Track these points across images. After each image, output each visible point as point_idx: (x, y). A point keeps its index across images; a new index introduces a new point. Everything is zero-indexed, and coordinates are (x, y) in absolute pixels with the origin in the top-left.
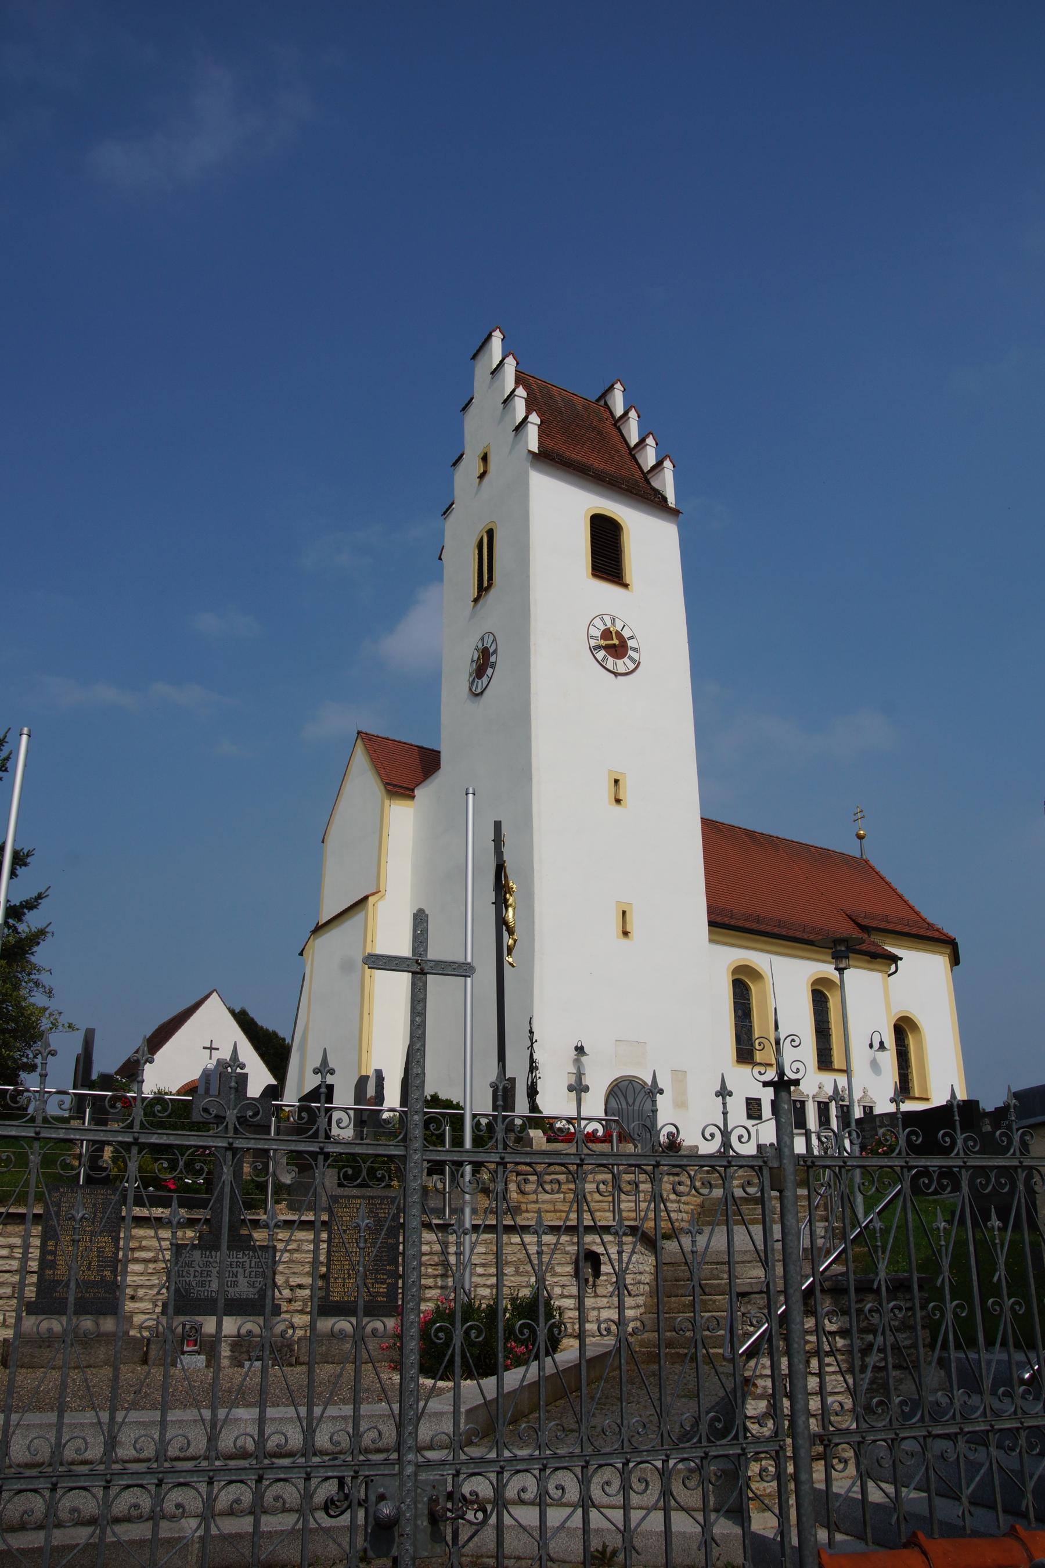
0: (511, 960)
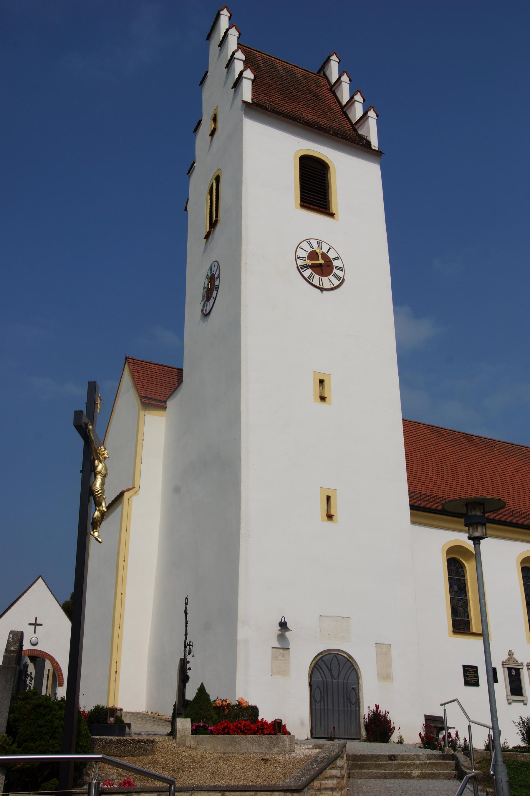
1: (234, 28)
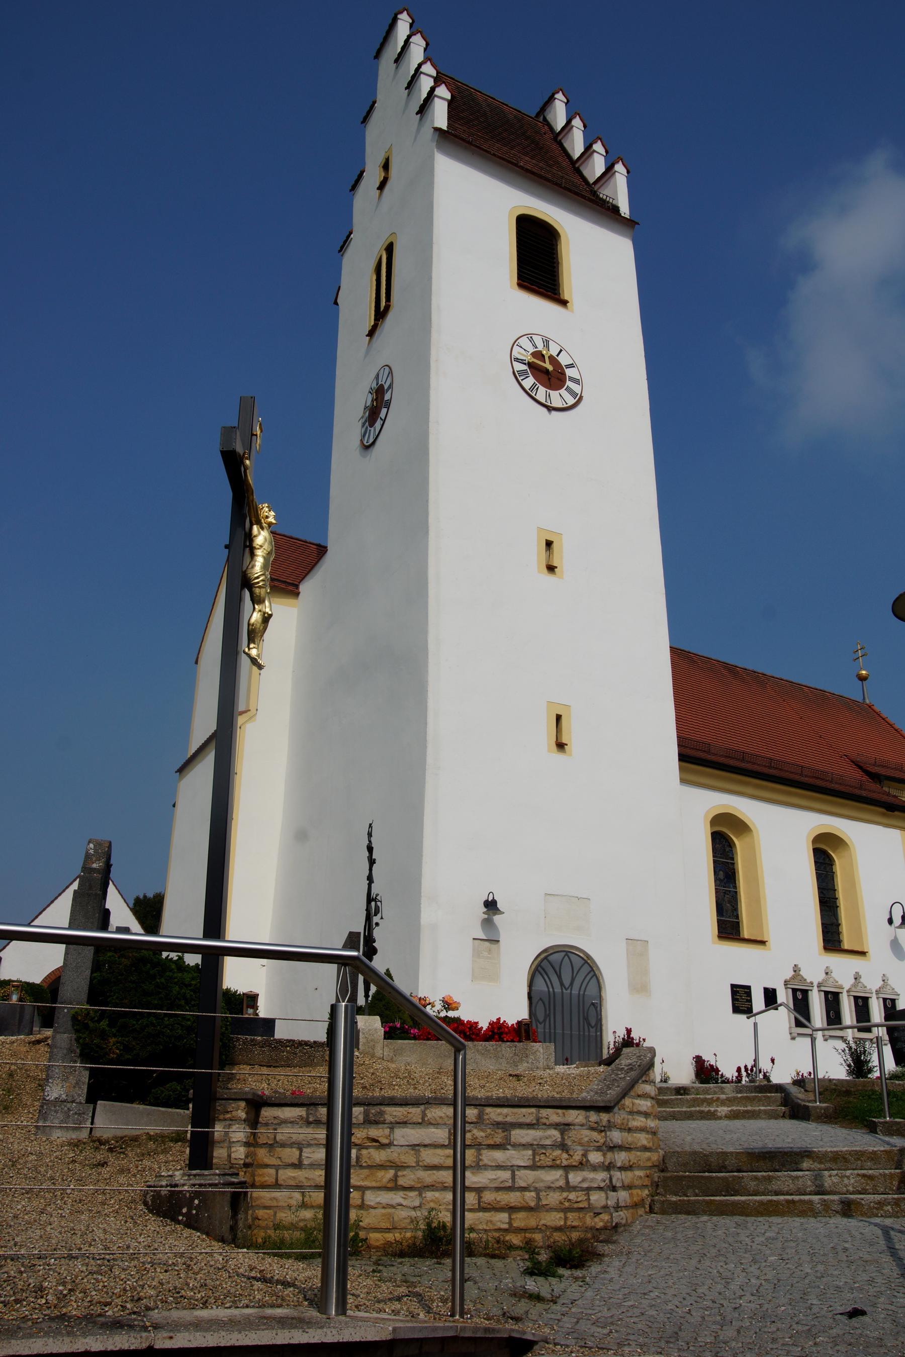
0: (254, 652)
1: (419, 35)
